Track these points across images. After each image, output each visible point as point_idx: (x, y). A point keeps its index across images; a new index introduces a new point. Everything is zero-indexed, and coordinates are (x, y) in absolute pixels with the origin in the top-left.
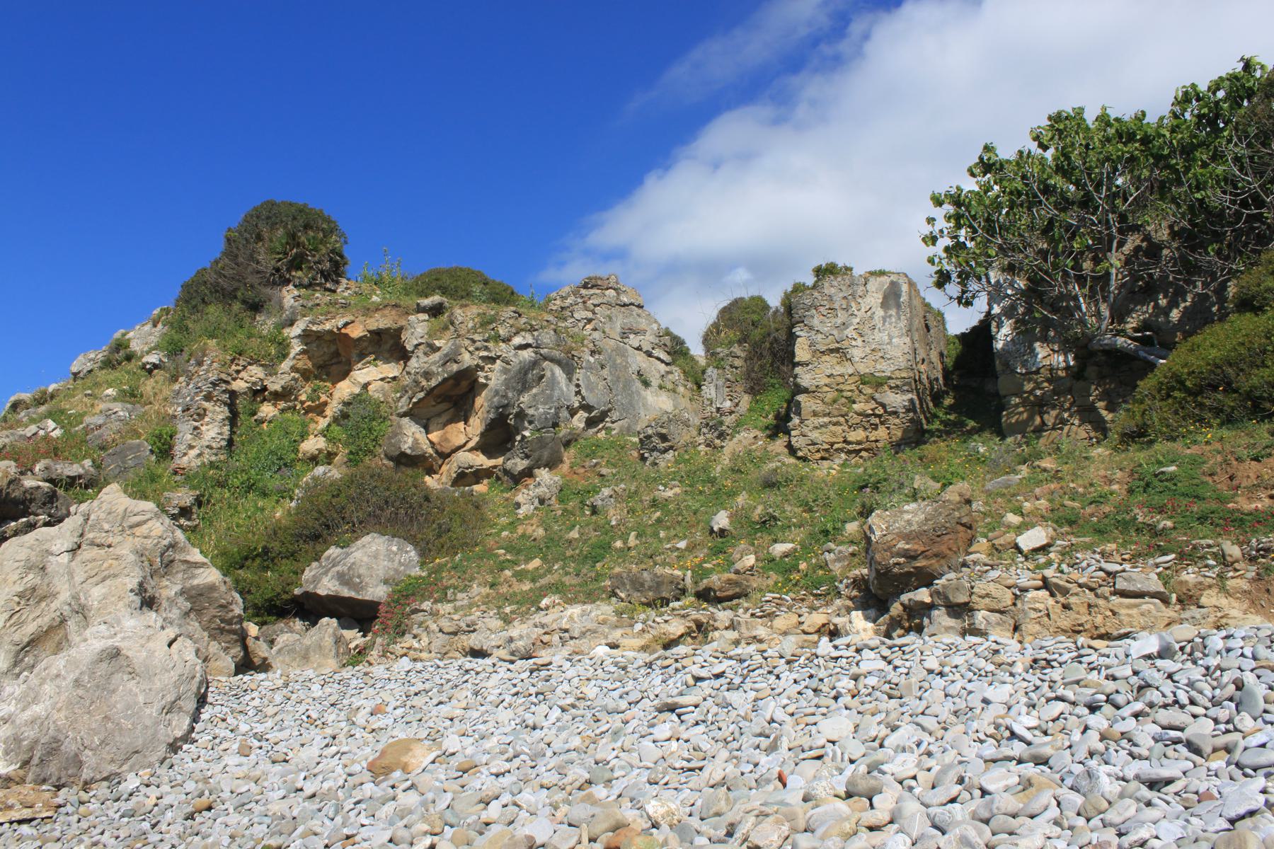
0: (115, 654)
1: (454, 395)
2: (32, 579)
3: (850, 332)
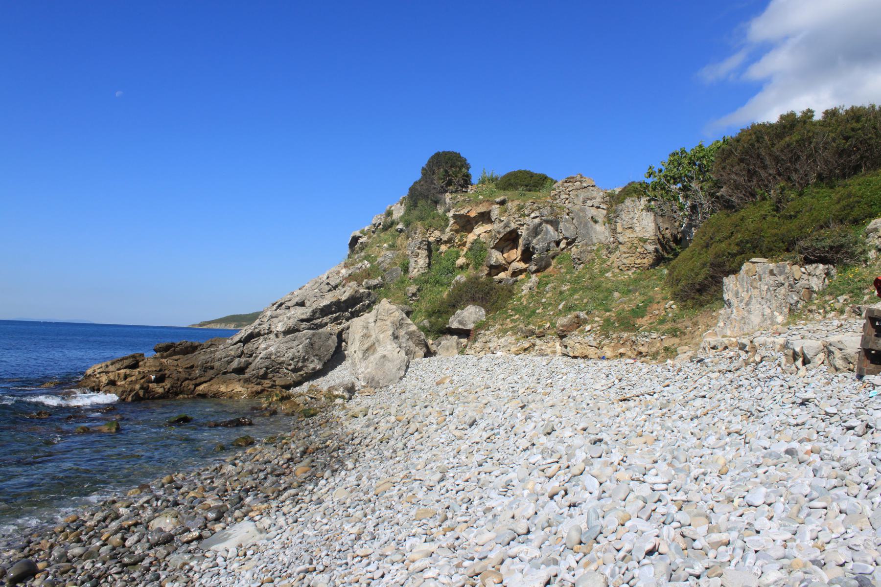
0: (384, 356)
1: (510, 240)
2: (365, 331)
3: (635, 221)
